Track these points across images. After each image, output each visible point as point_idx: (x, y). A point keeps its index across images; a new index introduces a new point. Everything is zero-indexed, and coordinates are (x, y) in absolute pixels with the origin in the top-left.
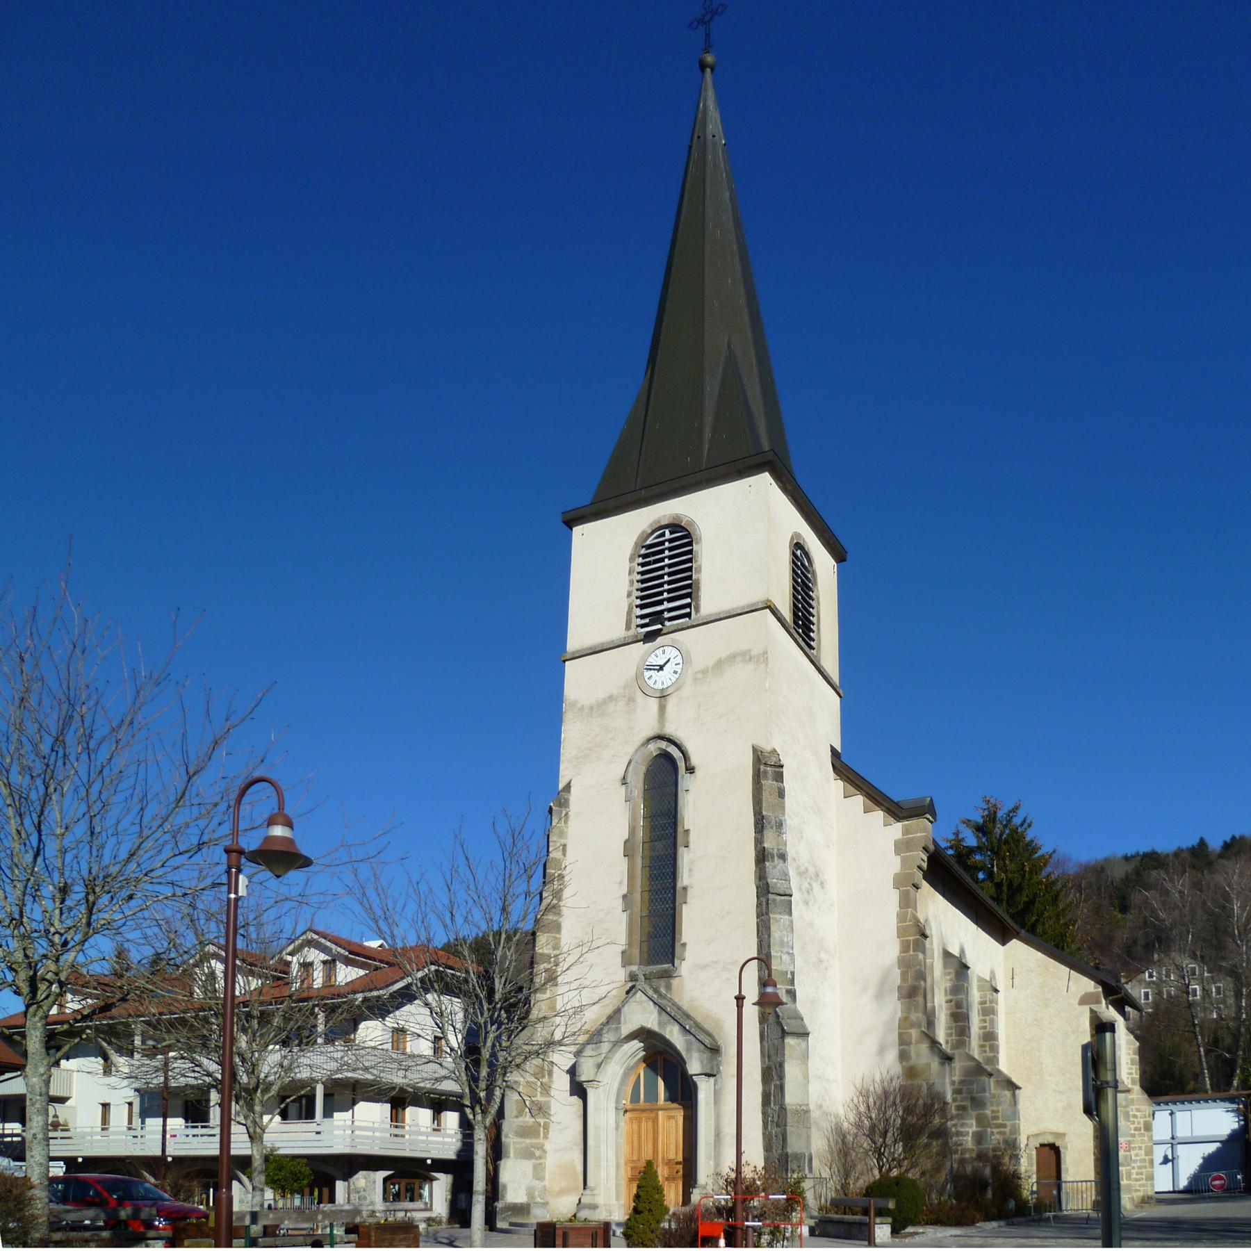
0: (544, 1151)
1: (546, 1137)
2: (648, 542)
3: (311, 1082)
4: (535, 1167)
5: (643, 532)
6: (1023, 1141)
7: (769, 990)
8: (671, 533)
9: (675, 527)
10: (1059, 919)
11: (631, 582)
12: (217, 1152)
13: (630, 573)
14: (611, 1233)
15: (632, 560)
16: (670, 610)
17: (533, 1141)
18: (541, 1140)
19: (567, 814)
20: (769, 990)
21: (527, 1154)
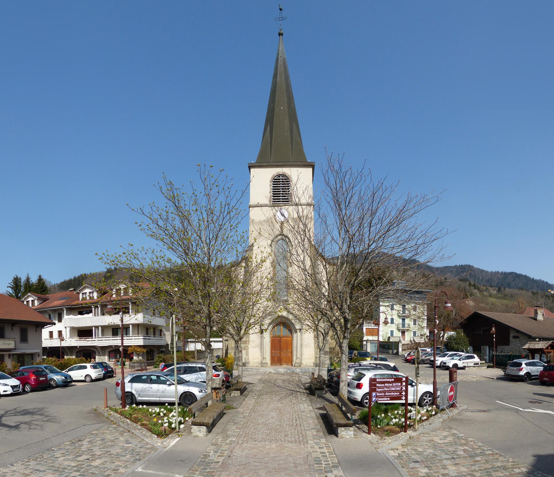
0: (248, 348)
1: (249, 344)
2: (275, 178)
3: (129, 325)
4: (246, 352)
5: (274, 175)
6: (47, 295)
7: (386, 320)
8: (282, 177)
9: (284, 175)
10: (230, 321)
11: (271, 188)
12: (433, 359)
13: (270, 186)
14: (149, 323)
15: (270, 182)
16: (282, 199)
17: (246, 345)
18: (247, 345)
19: (252, 253)
20: (386, 320)
21: (245, 349)
